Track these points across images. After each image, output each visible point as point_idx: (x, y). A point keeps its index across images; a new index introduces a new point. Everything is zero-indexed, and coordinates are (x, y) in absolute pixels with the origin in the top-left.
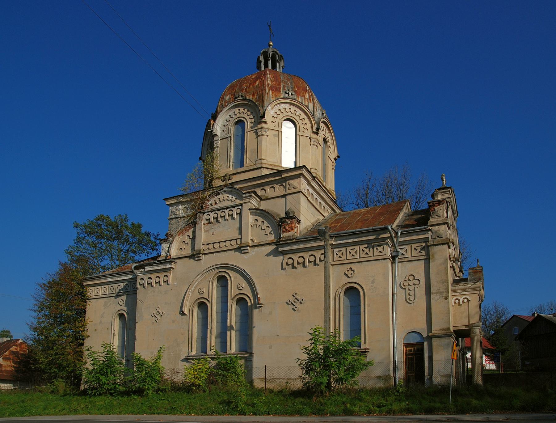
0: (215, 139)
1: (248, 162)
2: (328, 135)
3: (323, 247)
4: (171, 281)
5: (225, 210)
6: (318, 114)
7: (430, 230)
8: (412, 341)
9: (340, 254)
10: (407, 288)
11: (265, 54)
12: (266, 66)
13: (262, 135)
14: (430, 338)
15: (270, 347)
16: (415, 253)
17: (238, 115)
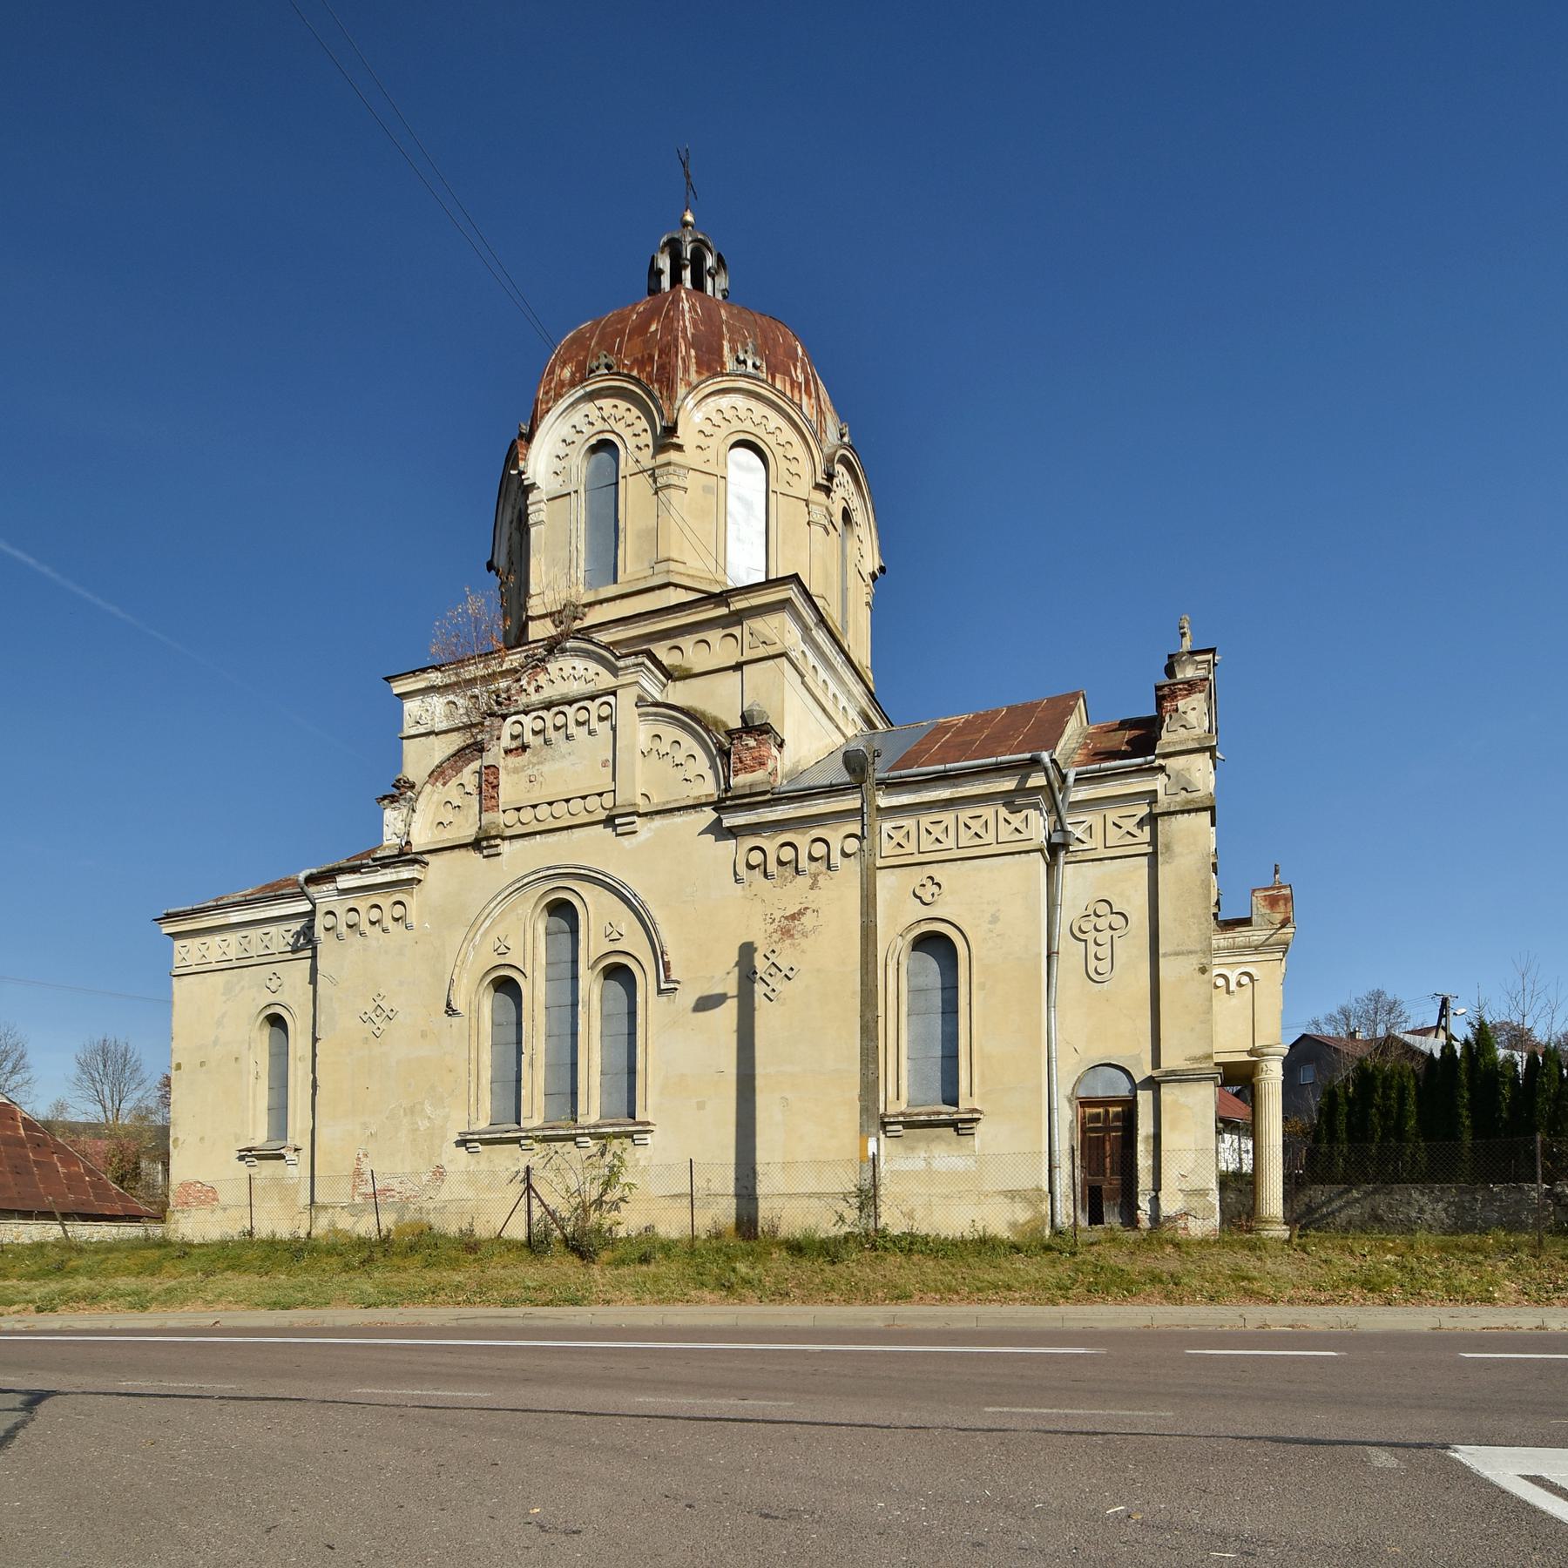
0: (532, 498)
1: (632, 568)
2: (855, 502)
3: (859, 812)
4: (412, 918)
5: (565, 708)
6: (832, 436)
7: (1162, 769)
8: (1100, 1092)
9: (899, 836)
10: (1090, 937)
11: (674, 247)
12: (676, 279)
13: (668, 486)
14: (1153, 1084)
15: (701, 1106)
16: (1114, 836)
17: (599, 425)
